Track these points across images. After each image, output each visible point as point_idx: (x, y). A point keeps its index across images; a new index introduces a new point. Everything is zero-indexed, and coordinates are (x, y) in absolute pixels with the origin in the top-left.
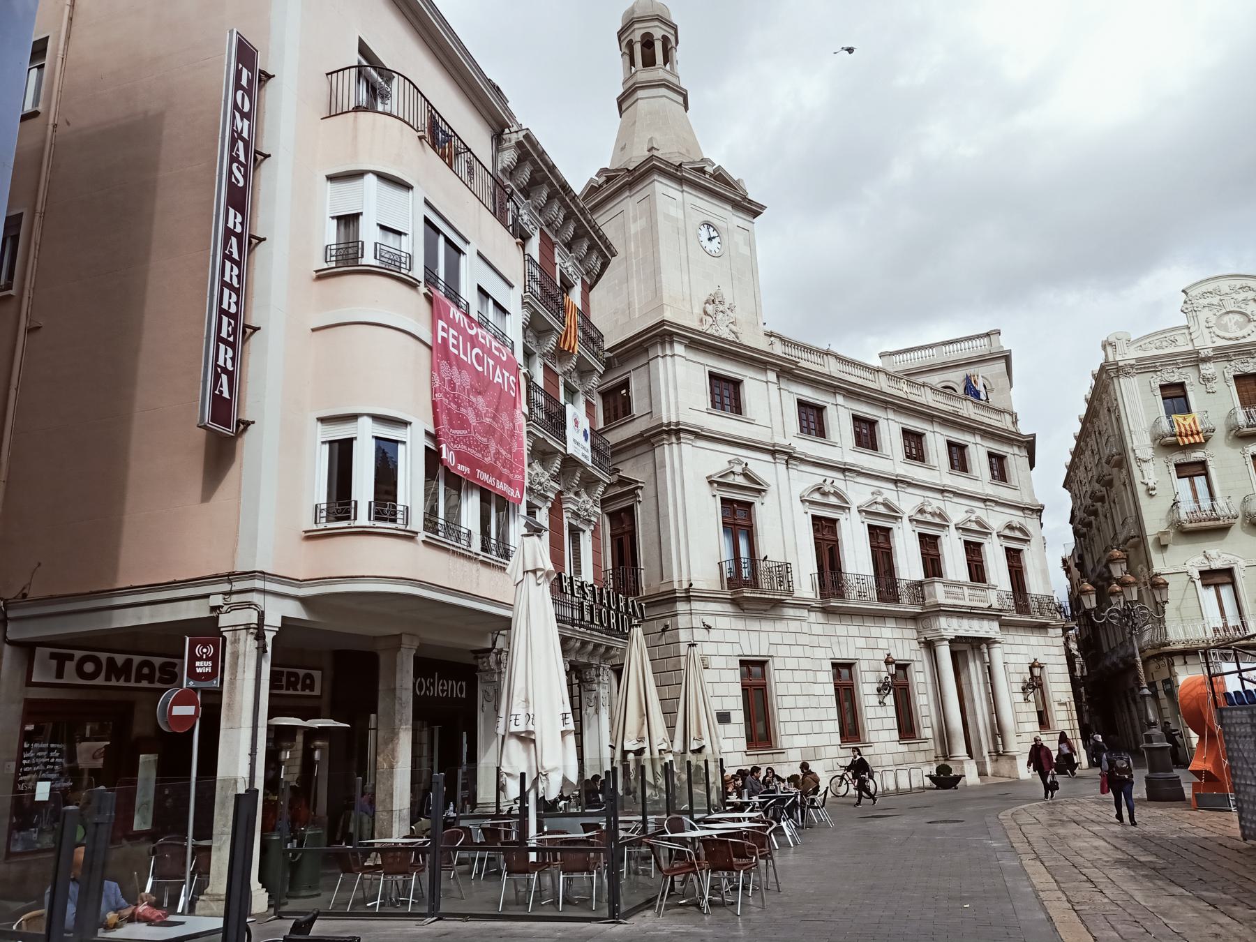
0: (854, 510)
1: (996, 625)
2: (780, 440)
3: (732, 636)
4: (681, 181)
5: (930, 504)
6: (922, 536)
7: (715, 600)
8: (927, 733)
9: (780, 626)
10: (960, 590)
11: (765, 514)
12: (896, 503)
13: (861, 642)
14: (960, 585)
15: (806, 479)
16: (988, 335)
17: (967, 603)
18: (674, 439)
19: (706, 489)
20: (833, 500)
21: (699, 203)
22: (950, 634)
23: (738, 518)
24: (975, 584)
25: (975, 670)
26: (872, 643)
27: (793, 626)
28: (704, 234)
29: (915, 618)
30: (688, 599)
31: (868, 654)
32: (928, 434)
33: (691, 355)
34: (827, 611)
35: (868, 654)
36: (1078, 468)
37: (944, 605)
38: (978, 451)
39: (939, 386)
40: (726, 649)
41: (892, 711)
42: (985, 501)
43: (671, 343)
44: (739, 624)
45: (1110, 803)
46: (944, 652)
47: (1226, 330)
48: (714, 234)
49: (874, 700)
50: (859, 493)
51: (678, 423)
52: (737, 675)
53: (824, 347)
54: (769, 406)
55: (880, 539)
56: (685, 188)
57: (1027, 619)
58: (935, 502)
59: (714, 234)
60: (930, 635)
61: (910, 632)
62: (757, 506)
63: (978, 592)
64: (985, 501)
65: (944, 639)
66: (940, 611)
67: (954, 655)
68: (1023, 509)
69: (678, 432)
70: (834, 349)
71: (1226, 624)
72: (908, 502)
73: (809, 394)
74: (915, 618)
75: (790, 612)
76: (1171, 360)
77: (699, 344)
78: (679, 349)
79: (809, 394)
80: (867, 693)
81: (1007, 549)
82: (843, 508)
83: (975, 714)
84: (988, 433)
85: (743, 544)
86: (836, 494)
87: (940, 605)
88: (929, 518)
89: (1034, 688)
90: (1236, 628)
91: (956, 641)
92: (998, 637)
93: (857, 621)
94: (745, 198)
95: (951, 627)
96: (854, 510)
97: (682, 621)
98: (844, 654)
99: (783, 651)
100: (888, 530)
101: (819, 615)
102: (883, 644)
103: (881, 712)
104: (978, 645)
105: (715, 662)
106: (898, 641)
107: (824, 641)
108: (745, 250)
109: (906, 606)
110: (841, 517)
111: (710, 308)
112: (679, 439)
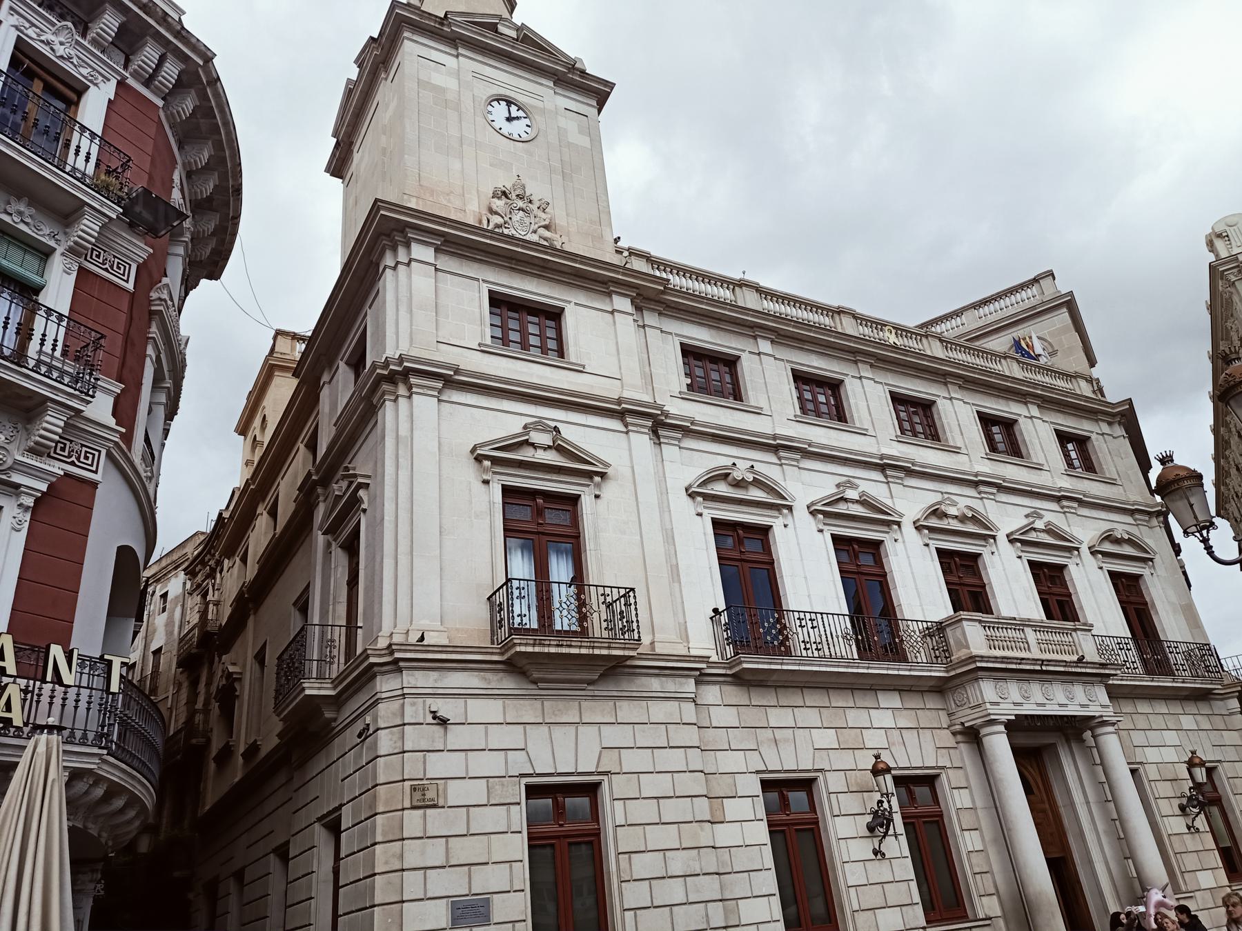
0: (801, 512)
1: (1101, 695)
2: (636, 392)
3: (512, 737)
4: (454, 41)
5: (954, 504)
6: (944, 556)
8: (987, 906)
9: (628, 711)
10: (1017, 635)
11: (603, 519)
12: (889, 502)
13: (827, 738)
14: (1021, 624)
15: (690, 463)
16: (1036, 280)
17: (1036, 653)
18: (402, 390)
19: (469, 473)
20: (756, 494)
21: (488, 71)
22: (1007, 711)
23: (543, 517)
24: (1055, 623)
25: (1072, 774)
26: (850, 737)
27: (660, 711)
28: (500, 110)
29: (940, 688)
30: (396, 666)
31: (844, 760)
32: (940, 402)
33: (446, 263)
34: (742, 680)
35: (844, 760)
36: (1228, 474)
37: (982, 658)
38: (1038, 431)
40: (491, 764)
41: (906, 869)
42: (1058, 499)
43: (408, 246)
44: (528, 710)
45: (425, 814)
46: (999, 746)
48: (515, 113)
49: (863, 849)
50: (807, 485)
51: (401, 359)
52: (519, 816)
53: (736, 275)
54: (610, 347)
55: (862, 566)
56: (461, 51)
57: (1167, 683)
58: (963, 501)
59: (514, 112)
60: (969, 718)
61: (931, 713)
62: (587, 502)
63: (1057, 638)
64: (1058, 499)
65: (993, 722)
66: (975, 671)
67: (1019, 754)
68: (1132, 512)
69: (406, 373)
70: (749, 277)
73: (702, 336)
74: (940, 688)
77: (459, 243)
78: (421, 252)
79: (702, 336)
80: (845, 835)
81: (1114, 576)
82: (777, 508)
83: (1090, 862)
84: (1049, 402)
85: (560, 570)
86: (757, 483)
87: (973, 659)
88: (955, 525)
89: (1202, 806)
91: (1018, 727)
92: (1108, 713)
93: (813, 698)
95: (1006, 700)
96: (801, 512)
98: (789, 760)
99: (633, 760)
100: (875, 547)
101: (728, 689)
102: (875, 739)
103: (880, 871)
104: (1074, 729)
105: (456, 793)
106: (901, 734)
107: (740, 739)
108: (584, 142)
109: (921, 663)
110: (777, 523)
111: (499, 204)
112: (410, 388)
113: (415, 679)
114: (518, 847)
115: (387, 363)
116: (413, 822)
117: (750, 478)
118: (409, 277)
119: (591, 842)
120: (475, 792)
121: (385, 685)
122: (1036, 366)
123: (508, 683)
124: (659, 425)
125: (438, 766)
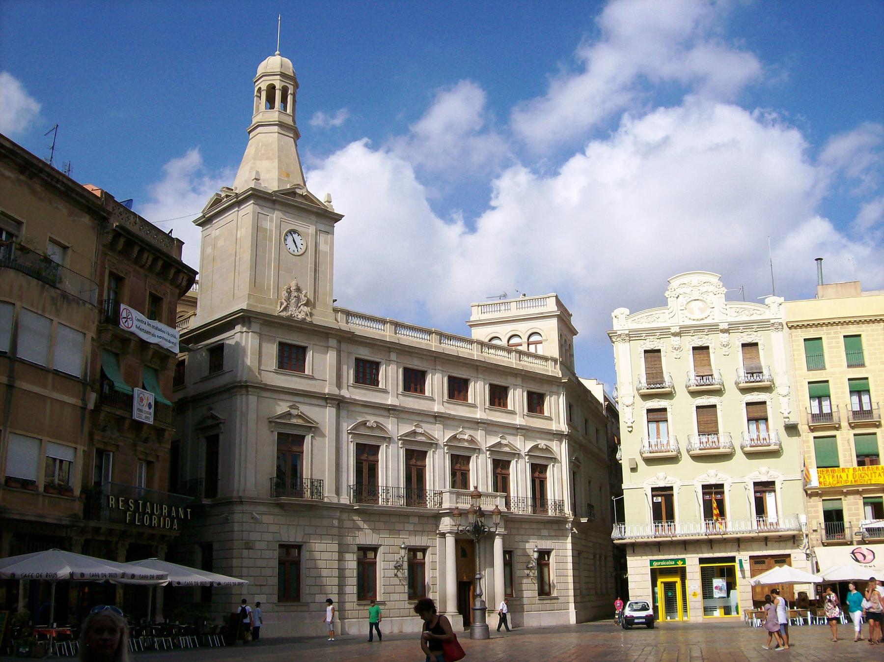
7: (263, 504)
30: (241, 503)
39: (486, 340)
40: (268, 537)
47: (692, 313)
51: (246, 381)
52: (276, 554)
54: (323, 367)
55: (415, 458)
69: (247, 387)
71: (758, 436)
72: (441, 434)
75: (325, 513)
76: (698, 329)
90: (764, 439)
94: (237, 195)
97: (237, 517)
105: (258, 545)
112: (248, 392)
113: (246, 508)
114: (275, 563)
115: (240, 382)
116: (245, 552)
117: (375, 425)
118: (247, 400)
119: (297, 563)
120: (263, 545)
121: (238, 508)
122: (421, 516)
123: (277, 510)
124: (340, 403)
125: (254, 536)
